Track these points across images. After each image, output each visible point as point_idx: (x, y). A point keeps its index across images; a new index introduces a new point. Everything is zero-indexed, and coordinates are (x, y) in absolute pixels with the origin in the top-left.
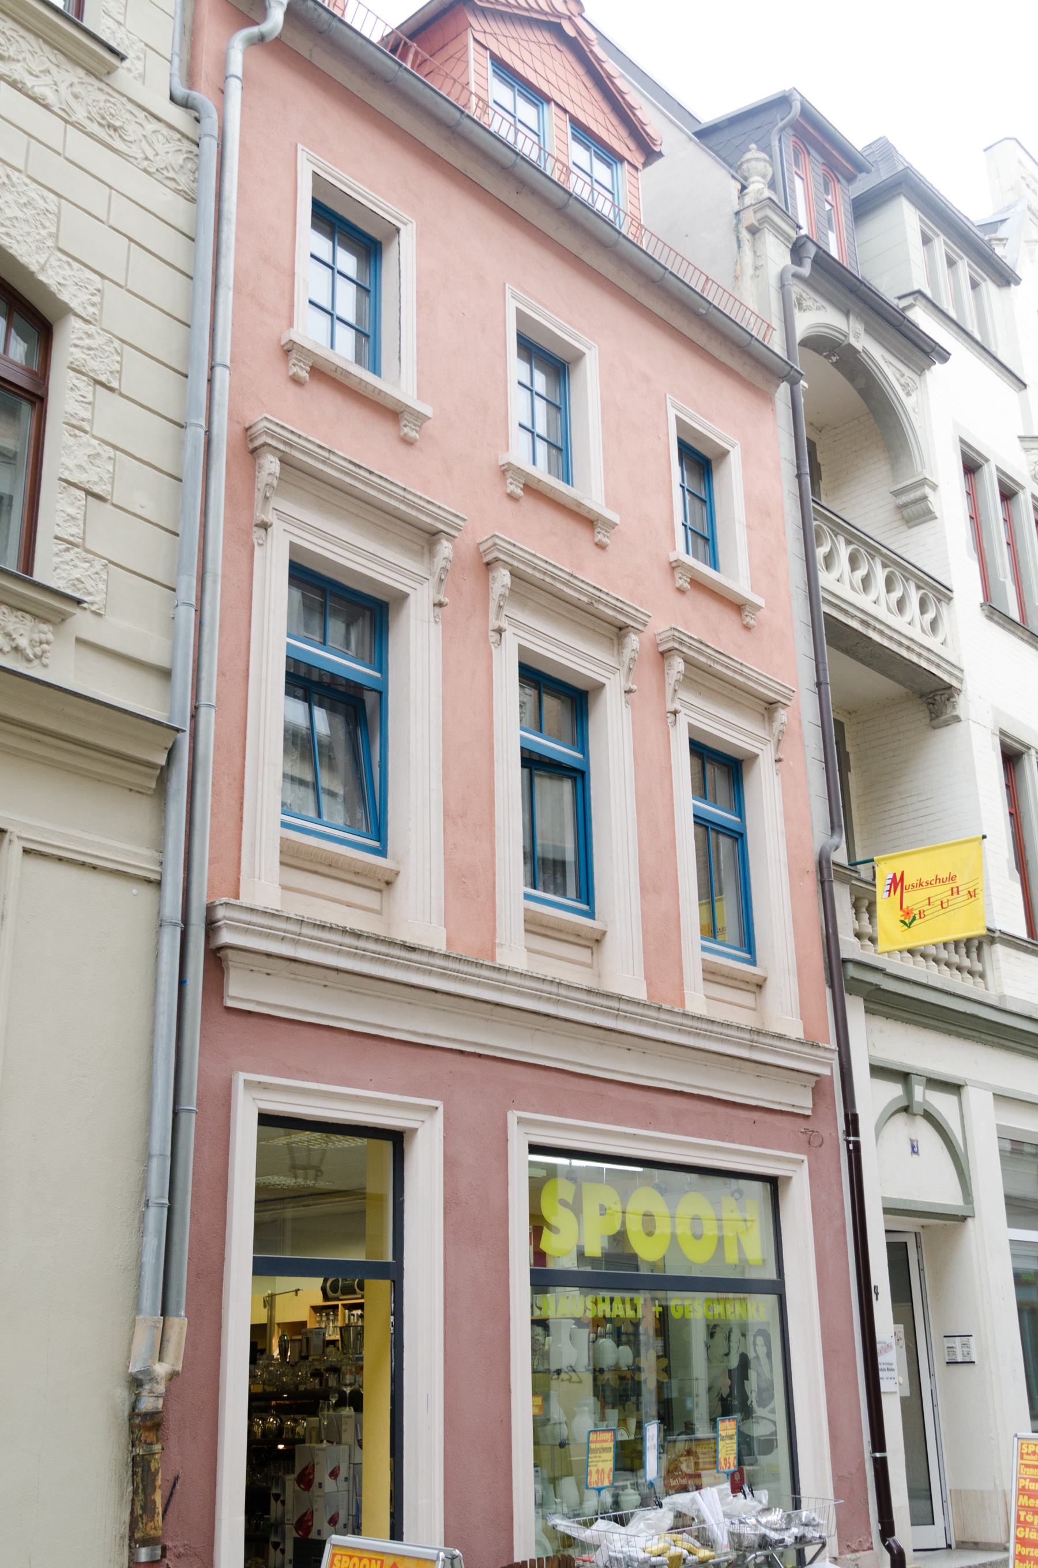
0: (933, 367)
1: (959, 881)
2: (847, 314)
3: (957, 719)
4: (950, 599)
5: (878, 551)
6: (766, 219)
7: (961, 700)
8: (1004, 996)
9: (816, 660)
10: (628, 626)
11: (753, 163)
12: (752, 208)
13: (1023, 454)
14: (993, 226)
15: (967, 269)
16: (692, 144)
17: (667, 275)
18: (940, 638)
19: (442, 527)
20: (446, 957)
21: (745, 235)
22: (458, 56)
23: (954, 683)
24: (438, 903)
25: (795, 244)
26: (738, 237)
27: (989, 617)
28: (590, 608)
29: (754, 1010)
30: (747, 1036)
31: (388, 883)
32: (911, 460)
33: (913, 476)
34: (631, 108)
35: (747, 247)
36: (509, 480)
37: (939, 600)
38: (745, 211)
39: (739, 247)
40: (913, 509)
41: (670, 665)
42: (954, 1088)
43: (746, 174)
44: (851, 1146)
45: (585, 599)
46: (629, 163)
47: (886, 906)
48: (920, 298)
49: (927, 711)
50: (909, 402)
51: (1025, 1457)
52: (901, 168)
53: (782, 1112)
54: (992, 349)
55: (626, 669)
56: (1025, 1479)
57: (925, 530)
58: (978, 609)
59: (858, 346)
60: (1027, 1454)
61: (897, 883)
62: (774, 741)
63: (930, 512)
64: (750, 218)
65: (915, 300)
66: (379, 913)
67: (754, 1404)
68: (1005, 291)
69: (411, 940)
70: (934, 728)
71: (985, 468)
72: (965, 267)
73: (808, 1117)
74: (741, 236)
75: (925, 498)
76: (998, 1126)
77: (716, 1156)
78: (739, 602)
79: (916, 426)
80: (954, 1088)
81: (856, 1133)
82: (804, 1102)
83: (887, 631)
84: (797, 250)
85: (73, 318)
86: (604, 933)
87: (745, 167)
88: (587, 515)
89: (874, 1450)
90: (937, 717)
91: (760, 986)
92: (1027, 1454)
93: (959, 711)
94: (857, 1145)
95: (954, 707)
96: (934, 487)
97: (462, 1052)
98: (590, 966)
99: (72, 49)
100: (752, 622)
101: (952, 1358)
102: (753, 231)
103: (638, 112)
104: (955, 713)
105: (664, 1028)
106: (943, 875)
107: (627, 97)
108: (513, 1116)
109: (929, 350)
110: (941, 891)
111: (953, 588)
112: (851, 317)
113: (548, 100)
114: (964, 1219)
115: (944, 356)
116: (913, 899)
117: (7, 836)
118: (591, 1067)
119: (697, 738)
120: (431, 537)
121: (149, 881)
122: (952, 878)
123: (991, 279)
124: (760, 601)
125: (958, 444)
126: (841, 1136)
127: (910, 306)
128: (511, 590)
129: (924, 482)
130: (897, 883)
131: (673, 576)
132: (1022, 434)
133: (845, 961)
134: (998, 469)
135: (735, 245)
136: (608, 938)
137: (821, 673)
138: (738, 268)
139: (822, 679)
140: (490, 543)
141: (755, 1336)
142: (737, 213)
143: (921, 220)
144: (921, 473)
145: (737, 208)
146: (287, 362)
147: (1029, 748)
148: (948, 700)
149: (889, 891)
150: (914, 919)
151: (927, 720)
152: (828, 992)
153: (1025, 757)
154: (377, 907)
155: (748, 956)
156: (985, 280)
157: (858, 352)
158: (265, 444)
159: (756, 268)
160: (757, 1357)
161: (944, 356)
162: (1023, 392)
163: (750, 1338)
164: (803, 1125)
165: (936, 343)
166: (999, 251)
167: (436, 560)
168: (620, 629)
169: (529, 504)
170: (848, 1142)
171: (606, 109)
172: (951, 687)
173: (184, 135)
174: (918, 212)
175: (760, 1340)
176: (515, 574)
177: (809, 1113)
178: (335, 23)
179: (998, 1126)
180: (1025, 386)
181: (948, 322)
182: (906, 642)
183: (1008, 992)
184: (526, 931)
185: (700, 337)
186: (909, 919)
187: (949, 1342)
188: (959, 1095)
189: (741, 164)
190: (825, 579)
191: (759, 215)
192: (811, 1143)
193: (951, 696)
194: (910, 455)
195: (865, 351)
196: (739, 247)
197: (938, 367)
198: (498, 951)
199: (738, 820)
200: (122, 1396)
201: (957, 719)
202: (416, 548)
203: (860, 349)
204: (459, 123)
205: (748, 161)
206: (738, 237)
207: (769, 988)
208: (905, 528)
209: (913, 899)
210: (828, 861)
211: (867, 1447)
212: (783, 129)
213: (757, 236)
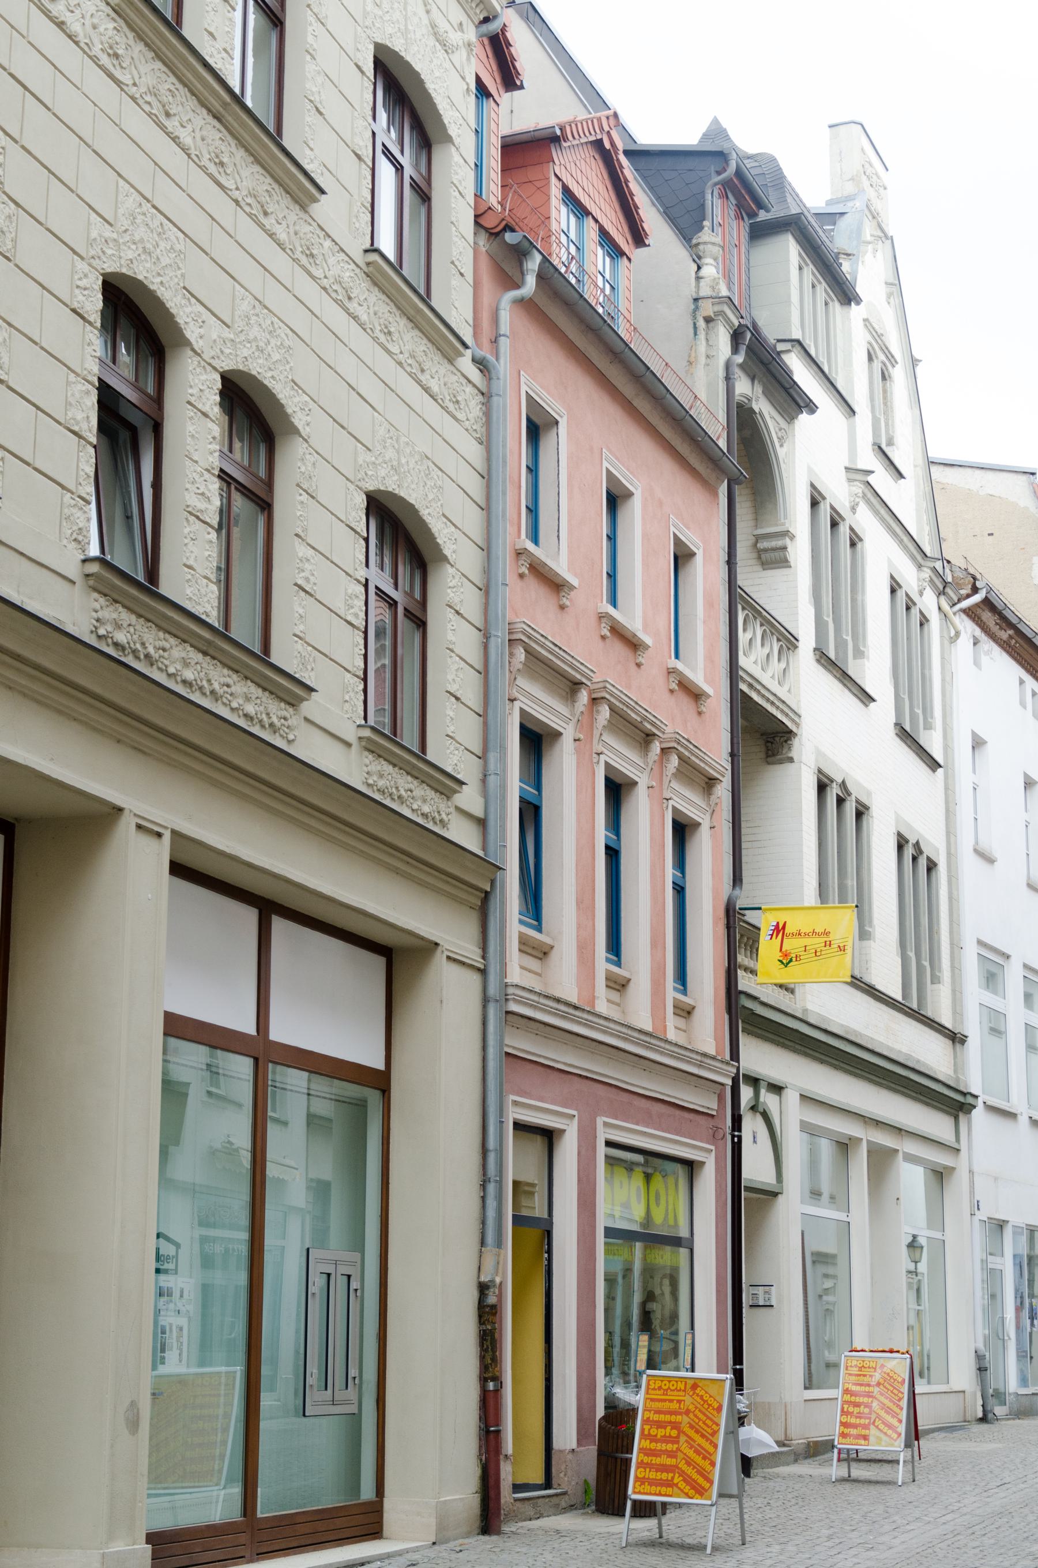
0: (800, 416)
1: (831, 937)
2: (753, 379)
3: (791, 760)
4: (796, 647)
5: (759, 613)
6: (722, 313)
7: (795, 742)
8: (807, 1010)
9: (732, 733)
10: (654, 735)
11: (709, 246)
12: (711, 300)
13: (846, 484)
14: (831, 218)
15: (811, 276)
16: (654, 209)
17: (688, 417)
18: (786, 687)
19: (584, 680)
20: (714, 1058)
21: (701, 324)
22: (538, 184)
23: (794, 729)
24: (575, 970)
25: (735, 332)
26: (695, 324)
27: (818, 661)
28: (639, 725)
29: (685, 1031)
30: (699, 1058)
31: (545, 953)
32: (776, 508)
33: (777, 525)
34: (636, 207)
35: (702, 335)
36: (603, 625)
37: (789, 649)
38: (704, 301)
39: (695, 334)
40: (772, 555)
41: (598, 712)
42: (777, 1089)
43: (701, 254)
44: (736, 1140)
45: (639, 719)
46: (593, 217)
47: (768, 947)
48: (797, 346)
49: (764, 749)
50: (781, 452)
51: (650, 1391)
52: (794, 210)
53: (703, 1113)
54: (832, 376)
55: (576, 719)
56: (650, 1411)
57: (776, 575)
58: (811, 653)
59: (756, 407)
60: (654, 1389)
61: (779, 930)
62: (710, 811)
63: (787, 561)
64: (707, 309)
65: (793, 346)
66: (539, 975)
67: (658, 1328)
68: (846, 308)
69: (558, 994)
70: (769, 763)
71: (822, 505)
72: (822, 288)
73: (713, 1116)
74: (698, 324)
75: (784, 548)
76: (802, 1121)
77: (677, 1147)
78: (558, 581)
79: (784, 475)
80: (777, 1089)
81: (740, 1130)
82: (707, 1102)
83: (763, 691)
84: (736, 337)
85: (448, 566)
86: (629, 980)
87: (701, 247)
88: (631, 638)
89: (735, 1364)
90: (774, 755)
91: (689, 1013)
92: (654, 1389)
93: (794, 754)
94: (740, 1138)
95: (790, 749)
96: (792, 537)
97: (580, 1076)
98: (618, 1005)
99: (447, 348)
100: (568, 603)
101: (755, 1302)
102: (708, 320)
103: (640, 211)
104: (790, 755)
105: (612, 1035)
106: (819, 929)
107: (635, 198)
108: (600, 1120)
109: (802, 404)
110: (817, 942)
111: (800, 638)
112: (756, 382)
113: (588, 213)
114: (775, 1194)
115: (811, 407)
116: (789, 944)
117: (440, 948)
118: (540, 1056)
119: (611, 776)
120: (574, 686)
121: (479, 970)
122: (826, 933)
123: (839, 301)
124: (574, 581)
125: (809, 488)
126: (728, 1131)
127: (788, 351)
128: (524, 664)
129: (786, 534)
130: (779, 930)
131: (517, 560)
132: (848, 465)
133: (741, 992)
134: (832, 508)
135: (692, 331)
136: (632, 984)
137: (735, 746)
138: (693, 355)
139: (736, 751)
140: (601, 685)
141: (662, 1279)
142: (696, 300)
143: (800, 254)
144: (783, 524)
145: (695, 296)
146: (517, 560)
147: (832, 781)
148: (786, 741)
149: (772, 935)
150: (791, 961)
151: (763, 755)
152: (727, 1017)
153: (828, 788)
154: (684, 1028)
155: (535, 923)
156: (833, 300)
157: (755, 413)
158: (603, 698)
159: (708, 356)
160: (663, 1294)
161: (811, 407)
162: (851, 420)
163: (657, 1279)
164: (711, 1122)
165: (811, 400)
166: (846, 267)
167: (576, 704)
168: (648, 735)
169: (532, 582)
170: (733, 1136)
171: (616, 205)
172: (791, 732)
173: (479, 390)
174: (799, 247)
175: (666, 1282)
176: (613, 709)
177: (714, 1113)
178: (581, 302)
179: (802, 1121)
180: (854, 412)
181: (832, 389)
182: (772, 698)
183: (810, 1006)
184: (607, 986)
185: (684, 449)
186: (786, 960)
187: (753, 1290)
188: (780, 1095)
189: (698, 244)
190: (743, 661)
191: (717, 308)
192: (714, 1137)
193: (789, 739)
194: (775, 503)
195: (761, 414)
196: (695, 334)
197: (804, 417)
198: (597, 1002)
199: (536, 792)
200: (474, 1294)
201: (791, 760)
202: (564, 694)
203: (757, 411)
204: (664, 398)
205: (705, 243)
206: (695, 324)
207: (697, 1014)
208: (759, 568)
209: (789, 944)
210: (734, 910)
211: (730, 1362)
212: (716, 184)
213: (711, 325)
